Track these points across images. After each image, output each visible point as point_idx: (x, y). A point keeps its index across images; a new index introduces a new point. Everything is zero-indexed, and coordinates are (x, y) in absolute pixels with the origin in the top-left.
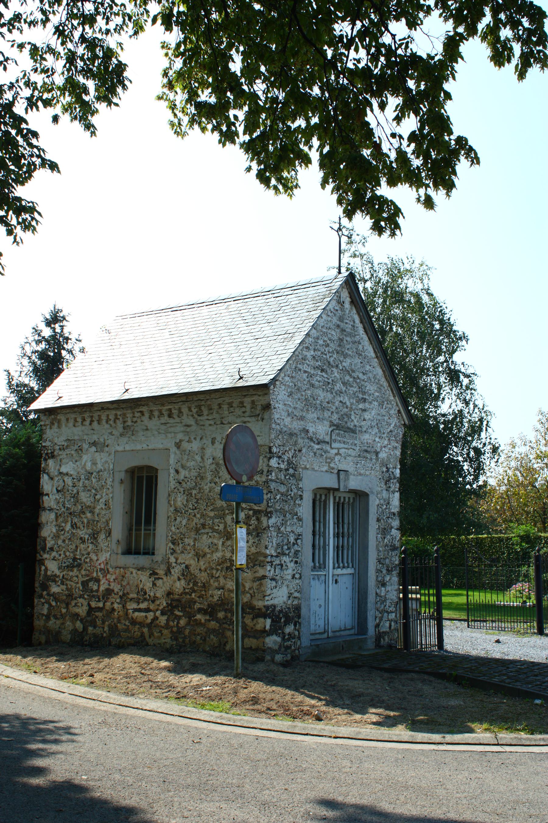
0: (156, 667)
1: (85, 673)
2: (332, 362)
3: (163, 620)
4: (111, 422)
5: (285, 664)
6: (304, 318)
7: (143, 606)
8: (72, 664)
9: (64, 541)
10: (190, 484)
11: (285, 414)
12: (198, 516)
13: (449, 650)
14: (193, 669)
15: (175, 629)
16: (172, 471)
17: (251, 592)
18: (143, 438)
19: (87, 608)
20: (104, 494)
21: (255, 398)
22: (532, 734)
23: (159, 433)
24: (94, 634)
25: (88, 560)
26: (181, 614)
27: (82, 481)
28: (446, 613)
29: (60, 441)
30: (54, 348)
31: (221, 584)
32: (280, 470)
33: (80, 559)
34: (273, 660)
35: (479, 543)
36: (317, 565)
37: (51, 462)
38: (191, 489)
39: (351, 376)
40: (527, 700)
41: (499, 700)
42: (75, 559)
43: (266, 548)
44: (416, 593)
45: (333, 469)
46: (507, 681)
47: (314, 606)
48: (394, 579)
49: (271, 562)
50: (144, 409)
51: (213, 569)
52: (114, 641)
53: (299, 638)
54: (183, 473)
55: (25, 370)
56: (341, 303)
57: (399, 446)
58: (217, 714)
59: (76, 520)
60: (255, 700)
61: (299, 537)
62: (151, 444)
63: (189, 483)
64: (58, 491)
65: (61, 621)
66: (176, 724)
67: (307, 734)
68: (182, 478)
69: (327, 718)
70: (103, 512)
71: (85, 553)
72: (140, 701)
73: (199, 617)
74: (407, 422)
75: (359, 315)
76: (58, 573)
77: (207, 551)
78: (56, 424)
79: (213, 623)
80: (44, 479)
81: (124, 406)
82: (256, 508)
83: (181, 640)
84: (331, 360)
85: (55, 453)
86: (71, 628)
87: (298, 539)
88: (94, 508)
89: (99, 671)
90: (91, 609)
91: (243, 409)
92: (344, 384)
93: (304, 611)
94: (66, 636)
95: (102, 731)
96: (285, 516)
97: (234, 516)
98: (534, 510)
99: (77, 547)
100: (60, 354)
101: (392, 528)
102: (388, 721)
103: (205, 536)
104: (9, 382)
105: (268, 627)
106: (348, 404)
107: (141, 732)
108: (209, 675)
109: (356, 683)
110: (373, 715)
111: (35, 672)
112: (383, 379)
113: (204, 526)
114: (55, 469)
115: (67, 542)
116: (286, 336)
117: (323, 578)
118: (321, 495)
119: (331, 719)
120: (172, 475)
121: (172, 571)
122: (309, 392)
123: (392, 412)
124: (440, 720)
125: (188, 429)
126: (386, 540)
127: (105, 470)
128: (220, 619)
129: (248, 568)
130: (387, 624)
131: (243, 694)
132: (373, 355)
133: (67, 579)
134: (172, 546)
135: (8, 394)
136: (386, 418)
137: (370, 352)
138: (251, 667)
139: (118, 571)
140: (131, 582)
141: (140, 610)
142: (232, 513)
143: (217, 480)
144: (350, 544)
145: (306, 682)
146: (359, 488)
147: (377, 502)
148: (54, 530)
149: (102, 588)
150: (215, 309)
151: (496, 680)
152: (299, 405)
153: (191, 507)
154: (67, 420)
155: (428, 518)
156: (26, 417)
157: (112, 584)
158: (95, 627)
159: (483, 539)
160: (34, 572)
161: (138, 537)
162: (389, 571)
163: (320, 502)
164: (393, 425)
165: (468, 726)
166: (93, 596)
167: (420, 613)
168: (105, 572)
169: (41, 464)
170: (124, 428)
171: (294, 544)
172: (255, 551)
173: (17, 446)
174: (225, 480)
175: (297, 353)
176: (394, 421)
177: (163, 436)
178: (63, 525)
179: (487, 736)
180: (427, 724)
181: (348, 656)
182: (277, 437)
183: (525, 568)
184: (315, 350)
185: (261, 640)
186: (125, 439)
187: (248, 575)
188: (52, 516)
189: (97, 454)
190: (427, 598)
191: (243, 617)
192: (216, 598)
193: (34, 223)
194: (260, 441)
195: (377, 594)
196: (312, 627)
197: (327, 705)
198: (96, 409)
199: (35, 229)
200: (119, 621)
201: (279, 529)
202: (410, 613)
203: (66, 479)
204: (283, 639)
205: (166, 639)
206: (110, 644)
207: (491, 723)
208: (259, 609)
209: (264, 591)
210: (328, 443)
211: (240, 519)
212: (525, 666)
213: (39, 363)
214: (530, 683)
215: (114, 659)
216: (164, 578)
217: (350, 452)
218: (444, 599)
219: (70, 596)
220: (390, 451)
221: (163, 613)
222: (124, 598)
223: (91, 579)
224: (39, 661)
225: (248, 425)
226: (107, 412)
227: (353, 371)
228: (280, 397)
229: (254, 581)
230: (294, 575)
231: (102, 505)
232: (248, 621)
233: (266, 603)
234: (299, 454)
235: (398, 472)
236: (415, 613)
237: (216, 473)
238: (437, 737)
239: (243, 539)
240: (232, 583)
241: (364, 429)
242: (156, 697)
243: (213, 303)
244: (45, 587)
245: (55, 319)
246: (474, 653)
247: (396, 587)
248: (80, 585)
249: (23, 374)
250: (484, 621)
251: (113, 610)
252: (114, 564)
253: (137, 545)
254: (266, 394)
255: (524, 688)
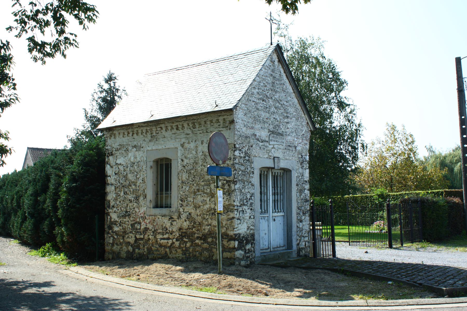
0: (174, 270)
1: (135, 274)
2: (268, 96)
3: (177, 244)
4: (144, 134)
5: (247, 266)
6: (252, 71)
7: (166, 236)
8: (127, 269)
9: (120, 202)
10: (190, 167)
11: (242, 125)
12: (195, 185)
13: (339, 257)
14: (195, 270)
15: (184, 249)
16: (180, 160)
17: (226, 226)
18: (162, 142)
19: (135, 239)
20: (142, 175)
21: (225, 117)
22: (387, 300)
23: (171, 139)
24: (139, 253)
25: (134, 212)
26: (187, 240)
27: (129, 168)
28: (337, 238)
29: (116, 146)
30: (111, 96)
31: (209, 223)
32: (241, 157)
33: (129, 212)
34: (240, 264)
35: (355, 199)
36: (263, 211)
37: (111, 158)
38: (190, 170)
39: (279, 103)
40: (384, 282)
41: (368, 283)
42: (126, 212)
43: (234, 201)
44: (320, 226)
45: (271, 156)
46: (372, 272)
47: (262, 234)
48: (307, 219)
49: (237, 209)
50: (163, 126)
51: (204, 214)
52: (150, 256)
53: (254, 252)
54: (186, 161)
55: (95, 108)
56: (273, 62)
57: (308, 143)
58: (209, 294)
59: (126, 190)
60: (230, 286)
61: (252, 195)
62: (167, 145)
63: (189, 167)
64: (116, 174)
65: (120, 246)
66: (187, 300)
67: (260, 303)
68: (185, 164)
69: (271, 294)
70: (142, 185)
71: (132, 208)
72: (166, 288)
73: (197, 241)
74: (312, 129)
75: (283, 68)
76: (117, 220)
77: (201, 204)
78: (113, 136)
79: (205, 244)
80: (108, 168)
81: (151, 124)
82: (228, 179)
83: (188, 255)
84: (268, 94)
85: (113, 153)
86: (126, 250)
87: (252, 196)
88: (136, 183)
89: (142, 273)
90: (136, 240)
91: (219, 124)
92: (276, 108)
93: (256, 237)
94: (123, 255)
95: (145, 304)
96: (244, 183)
97: (216, 184)
98: (386, 180)
99: (127, 205)
100: (114, 98)
101: (305, 189)
102: (305, 295)
103: (200, 196)
104: (86, 115)
105: (236, 246)
106: (278, 119)
107: (167, 304)
108: (204, 273)
109: (287, 276)
110: (297, 292)
111: (107, 274)
112: (298, 105)
113: (198, 190)
114: (113, 161)
115: (122, 202)
116: (242, 81)
117: (267, 218)
118: (264, 172)
119: (273, 295)
120: (179, 162)
121: (181, 216)
122: (256, 113)
123: (304, 123)
124: (335, 294)
125: (188, 136)
126: (302, 196)
127: (142, 161)
128: (209, 242)
129: (224, 213)
130: (304, 244)
131: (223, 283)
132: (292, 91)
133: (122, 223)
134: (181, 203)
135: (86, 122)
136: (300, 127)
137: (290, 89)
138: (227, 268)
139: (151, 217)
140: (159, 223)
141: (164, 239)
142: (214, 183)
143: (205, 164)
144: (282, 199)
145: (258, 276)
146: (286, 167)
147: (296, 175)
148: (114, 196)
149: (142, 227)
150: (201, 68)
151: (366, 272)
152: (251, 120)
153: (191, 180)
154: (119, 134)
155: (326, 185)
156: (96, 135)
157: (148, 225)
158: (139, 249)
159: (357, 197)
160: (104, 220)
161: (162, 198)
162: (304, 214)
163: (264, 175)
164: (304, 131)
165: (351, 297)
166: (138, 232)
167: (322, 237)
168: (144, 218)
169: (105, 159)
170: (151, 137)
171: (250, 199)
172: (228, 204)
173: (92, 149)
174: (210, 163)
175: (248, 91)
176: (305, 129)
177: (174, 141)
178: (119, 193)
179: (362, 302)
180: (327, 296)
181: (282, 261)
182: (238, 139)
183: (381, 213)
184: (258, 89)
185: (233, 253)
186: (152, 143)
187: (223, 217)
188: (113, 188)
189: (137, 152)
190: (326, 231)
191: (222, 241)
192: (207, 231)
193: (94, 18)
194: (229, 141)
195: (297, 226)
196: (262, 246)
197: (271, 287)
198: (135, 127)
199: (95, 21)
200: (153, 245)
201: (241, 191)
202: (317, 237)
203: (120, 167)
204: (245, 252)
205: (179, 254)
206: (148, 258)
207: (364, 294)
208: (231, 236)
209: (234, 226)
210: (267, 142)
211: (219, 185)
212: (383, 264)
213: (102, 104)
214: (386, 273)
215: (151, 267)
216: (177, 220)
217: (281, 146)
218: (336, 231)
219: (125, 232)
220: (303, 146)
221: (177, 240)
222: (155, 232)
223: (136, 223)
224: (109, 269)
225: (222, 132)
226: (142, 128)
227: (281, 101)
228: (239, 116)
229: (228, 221)
230: (250, 216)
231: (141, 181)
232: (225, 242)
233: (235, 233)
234: (251, 148)
235: (307, 158)
236: (319, 237)
237: (204, 160)
238: (333, 303)
239: (221, 197)
240: (215, 222)
241: (288, 134)
242: (175, 286)
243: (199, 65)
244: (110, 228)
245: (110, 79)
246: (353, 259)
247: (308, 223)
248: (130, 226)
249: (93, 111)
250: (358, 242)
251: (149, 239)
252: (149, 214)
253: (161, 203)
254: (231, 114)
255: (382, 275)
